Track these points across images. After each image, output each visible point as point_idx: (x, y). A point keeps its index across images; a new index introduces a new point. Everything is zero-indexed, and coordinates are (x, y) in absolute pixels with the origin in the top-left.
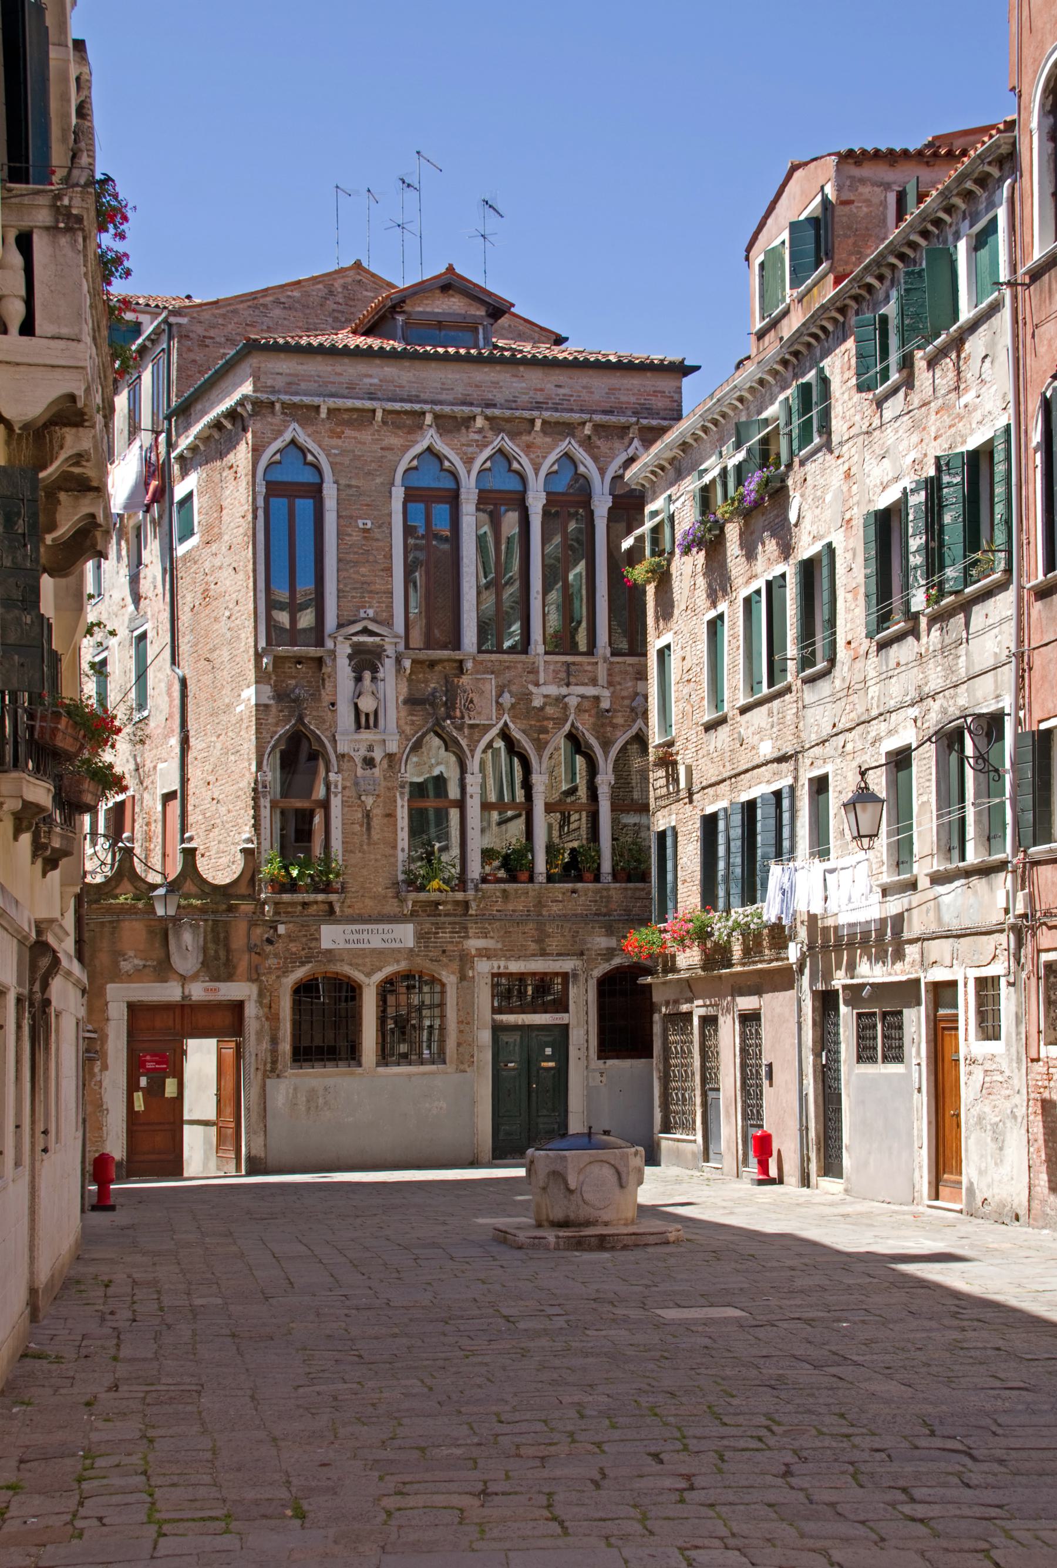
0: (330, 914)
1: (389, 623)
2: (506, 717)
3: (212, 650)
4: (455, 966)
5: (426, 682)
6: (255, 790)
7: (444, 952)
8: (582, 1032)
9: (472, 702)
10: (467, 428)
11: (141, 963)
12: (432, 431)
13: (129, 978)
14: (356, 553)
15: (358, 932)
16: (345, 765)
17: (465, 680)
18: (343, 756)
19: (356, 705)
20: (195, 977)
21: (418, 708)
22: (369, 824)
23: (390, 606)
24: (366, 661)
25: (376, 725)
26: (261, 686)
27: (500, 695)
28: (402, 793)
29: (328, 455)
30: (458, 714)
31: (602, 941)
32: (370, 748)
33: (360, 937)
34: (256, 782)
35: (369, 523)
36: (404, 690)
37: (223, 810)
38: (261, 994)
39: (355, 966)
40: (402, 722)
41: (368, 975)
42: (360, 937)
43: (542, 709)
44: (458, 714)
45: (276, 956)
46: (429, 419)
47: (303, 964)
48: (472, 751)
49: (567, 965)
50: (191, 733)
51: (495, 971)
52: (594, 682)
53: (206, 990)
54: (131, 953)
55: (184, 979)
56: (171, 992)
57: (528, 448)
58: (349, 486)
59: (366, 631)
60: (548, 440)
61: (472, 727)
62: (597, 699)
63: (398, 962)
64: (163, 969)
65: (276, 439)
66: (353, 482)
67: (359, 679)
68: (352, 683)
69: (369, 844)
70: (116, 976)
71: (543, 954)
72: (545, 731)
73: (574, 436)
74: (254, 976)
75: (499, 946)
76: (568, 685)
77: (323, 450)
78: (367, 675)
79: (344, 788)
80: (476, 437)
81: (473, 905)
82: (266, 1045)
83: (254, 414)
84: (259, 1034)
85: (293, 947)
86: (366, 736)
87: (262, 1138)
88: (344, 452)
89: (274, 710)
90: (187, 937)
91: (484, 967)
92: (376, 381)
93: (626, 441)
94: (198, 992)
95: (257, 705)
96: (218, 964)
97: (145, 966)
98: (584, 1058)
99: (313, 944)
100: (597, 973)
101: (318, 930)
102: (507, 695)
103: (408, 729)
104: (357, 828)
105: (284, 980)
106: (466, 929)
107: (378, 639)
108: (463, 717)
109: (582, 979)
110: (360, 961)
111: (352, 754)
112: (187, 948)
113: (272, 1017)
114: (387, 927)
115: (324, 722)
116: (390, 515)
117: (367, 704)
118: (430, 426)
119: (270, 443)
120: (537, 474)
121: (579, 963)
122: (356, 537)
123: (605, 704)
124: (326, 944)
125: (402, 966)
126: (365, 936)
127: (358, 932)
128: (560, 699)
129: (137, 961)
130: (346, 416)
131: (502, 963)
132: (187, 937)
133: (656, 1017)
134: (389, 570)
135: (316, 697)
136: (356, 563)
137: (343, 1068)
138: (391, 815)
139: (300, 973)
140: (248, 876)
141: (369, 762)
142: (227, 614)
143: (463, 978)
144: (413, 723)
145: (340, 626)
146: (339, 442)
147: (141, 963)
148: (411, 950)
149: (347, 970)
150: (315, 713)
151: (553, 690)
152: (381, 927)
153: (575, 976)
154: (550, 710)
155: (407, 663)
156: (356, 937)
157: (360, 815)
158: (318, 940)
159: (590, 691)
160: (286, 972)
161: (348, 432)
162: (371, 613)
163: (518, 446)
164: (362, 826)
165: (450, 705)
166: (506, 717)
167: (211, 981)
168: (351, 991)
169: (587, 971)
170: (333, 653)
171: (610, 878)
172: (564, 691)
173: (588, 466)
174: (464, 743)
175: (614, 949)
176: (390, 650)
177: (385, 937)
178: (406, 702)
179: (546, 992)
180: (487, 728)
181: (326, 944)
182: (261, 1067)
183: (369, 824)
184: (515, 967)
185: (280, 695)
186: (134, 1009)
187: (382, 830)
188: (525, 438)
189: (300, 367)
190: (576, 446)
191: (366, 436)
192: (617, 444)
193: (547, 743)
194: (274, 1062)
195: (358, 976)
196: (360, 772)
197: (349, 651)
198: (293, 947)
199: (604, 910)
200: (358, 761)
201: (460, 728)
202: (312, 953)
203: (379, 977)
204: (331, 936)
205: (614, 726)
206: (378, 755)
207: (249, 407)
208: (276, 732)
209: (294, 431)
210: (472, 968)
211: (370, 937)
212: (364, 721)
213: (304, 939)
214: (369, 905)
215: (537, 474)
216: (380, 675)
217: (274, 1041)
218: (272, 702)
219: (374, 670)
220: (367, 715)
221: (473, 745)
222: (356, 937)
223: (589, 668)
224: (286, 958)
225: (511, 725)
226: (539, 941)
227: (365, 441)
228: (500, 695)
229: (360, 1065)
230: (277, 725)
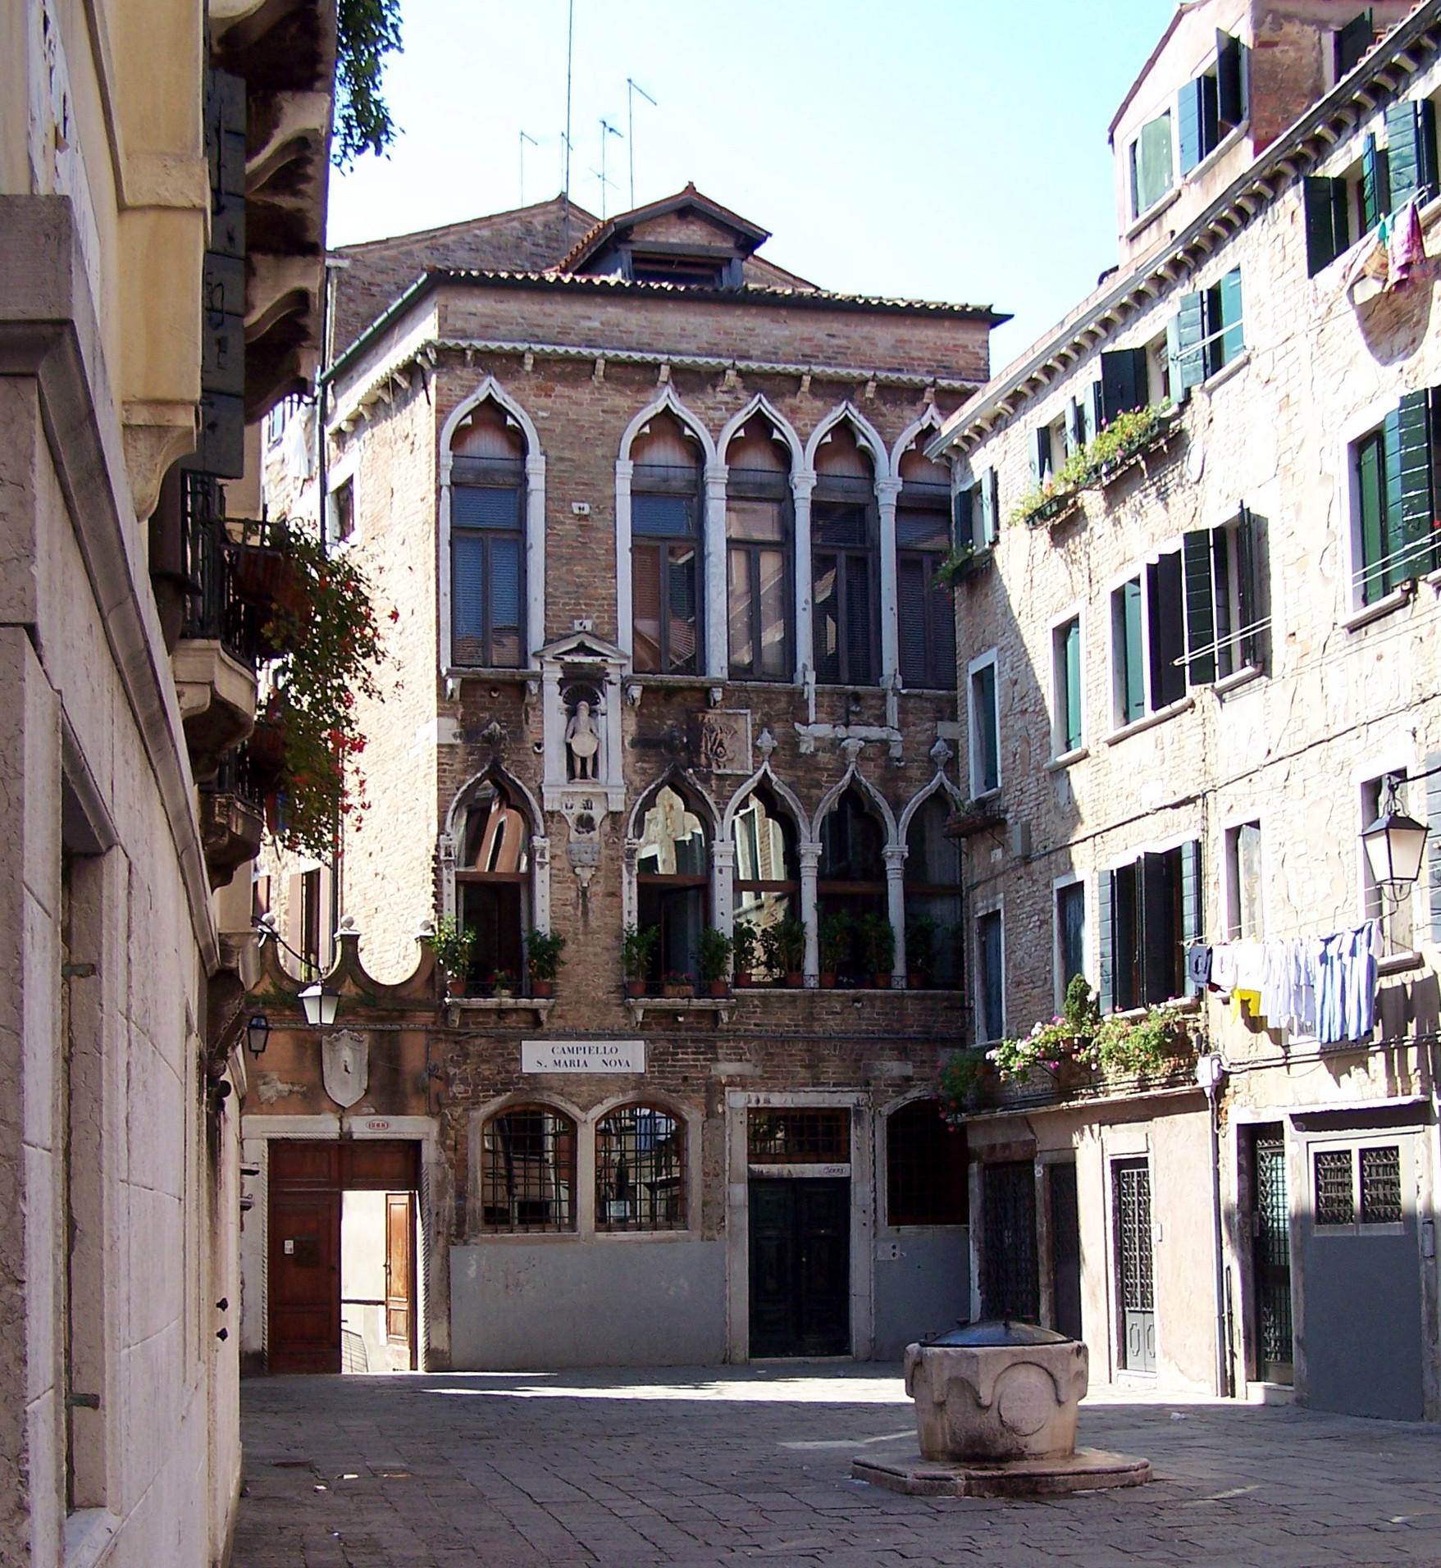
0: (535, 1026)
1: (611, 638)
4: (700, 1098)
5: (661, 717)
6: (435, 858)
7: (685, 1079)
8: (868, 1188)
9: (721, 745)
10: (714, 387)
11: (286, 1088)
12: (668, 390)
14: (569, 546)
15: (571, 1051)
16: (554, 827)
17: (711, 716)
18: (552, 813)
19: (569, 746)
20: (356, 1109)
21: (652, 752)
22: (585, 906)
23: (614, 619)
24: (582, 688)
25: (595, 774)
26: (444, 720)
29: (533, 419)
31: (893, 1068)
32: (588, 805)
33: (574, 1057)
34: (437, 848)
35: (586, 506)
36: (632, 725)
38: (443, 1132)
39: (569, 1096)
40: (629, 771)
42: (574, 1057)
43: (814, 755)
45: (464, 1081)
46: (665, 371)
47: (498, 1093)
48: (722, 811)
51: (753, 1105)
52: (882, 720)
54: (274, 1076)
55: (341, 1111)
56: (325, 1127)
57: (792, 413)
58: (561, 459)
59: (582, 649)
60: (819, 404)
62: (885, 744)
63: (623, 1091)
64: (313, 1097)
65: (466, 397)
66: (567, 454)
67: (572, 713)
68: (564, 718)
69: (585, 933)
72: (819, 786)
73: (851, 400)
75: (759, 1071)
76: (847, 725)
77: (528, 412)
78: (584, 706)
79: (553, 857)
80: (727, 398)
81: (725, 1016)
85: (486, 1070)
86: (580, 787)
87: (445, 1324)
88: (555, 415)
90: (347, 1054)
92: (596, 324)
93: (919, 406)
94: (362, 1127)
95: (439, 746)
96: (388, 1092)
97: (291, 1092)
98: (870, 1224)
99: (512, 1066)
100: (886, 1110)
102: (766, 735)
103: (637, 780)
105: (474, 1114)
106: (713, 1048)
108: (710, 765)
109: (867, 1117)
110: (573, 1089)
111: (564, 812)
113: (460, 1165)
114: (609, 1044)
115: (529, 768)
117: (584, 746)
118: (666, 383)
119: (458, 403)
120: (804, 448)
121: (861, 1095)
122: (570, 526)
123: (896, 752)
124: (529, 1066)
126: (581, 1056)
127: (571, 1051)
128: (835, 744)
129: (280, 1086)
130: (557, 370)
131: (762, 1096)
132: (347, 1054)
134: (613, 567)
135: (517, 735)
136: (570, 560)
138: (615, 894)
139: (494, 1104)
140: (426, 974)
141: (586, 823)
143: (710, 1114)
144: (644, 772)
146: (549, 402)
147: (286, 1088)
150: (514, 757)
151: (825, 730)
152: (601, 1044)
153: (859, 1113)
154: (823, 757)
155: (636, 692)
156: (568, 1057)
157: (574, 894)
158: (519, 1060)
159: (875, 733)
160: (476, 1104)
161: (559, 389)
163: (780, 411)
164: (576, 908)
166: (766, 765)
167: (377, 1113)
172: (841, 732)
173: (870, 436)
174: (710, 800)
175: (908, 1079)
176: (614, 675)
177: (607, 1058)
178: (633, 744)
180: (741, 780)
181: (529, 1066)
182: (444, 1230)
183: (585, 906)
185: (469, 732)
187: (603, 915)
188: (789, 401)
189: (500, 306)
190: (856, 412)
191: (584, 394)
192: (908, 412)
193: (820, 800)
194: (461, 1223)
195: (574, 1111)
196: (573, 835)
197: (560, 675)
199: (896, 1026)
201: (705, 780)
202: (511, 1078)
203: (598, 1111)
204: (537, 1056)
205: (909, 780)
206: (598, 813)
208: (463, 782)
209: (489, 386)
210: (722, 1102)
212: (579, 768)
213: (500, 1060)
214: (586, 1017)
215: (804, 448)
216: (601, 707)
218: (459, 741)
219: (594, 701)
220: (584, 760)
222: (568, 1057)
223: (873, 702)
224: (476, 1085)
225: (772, 776)
227: (585, 402)
230: (465, 771)
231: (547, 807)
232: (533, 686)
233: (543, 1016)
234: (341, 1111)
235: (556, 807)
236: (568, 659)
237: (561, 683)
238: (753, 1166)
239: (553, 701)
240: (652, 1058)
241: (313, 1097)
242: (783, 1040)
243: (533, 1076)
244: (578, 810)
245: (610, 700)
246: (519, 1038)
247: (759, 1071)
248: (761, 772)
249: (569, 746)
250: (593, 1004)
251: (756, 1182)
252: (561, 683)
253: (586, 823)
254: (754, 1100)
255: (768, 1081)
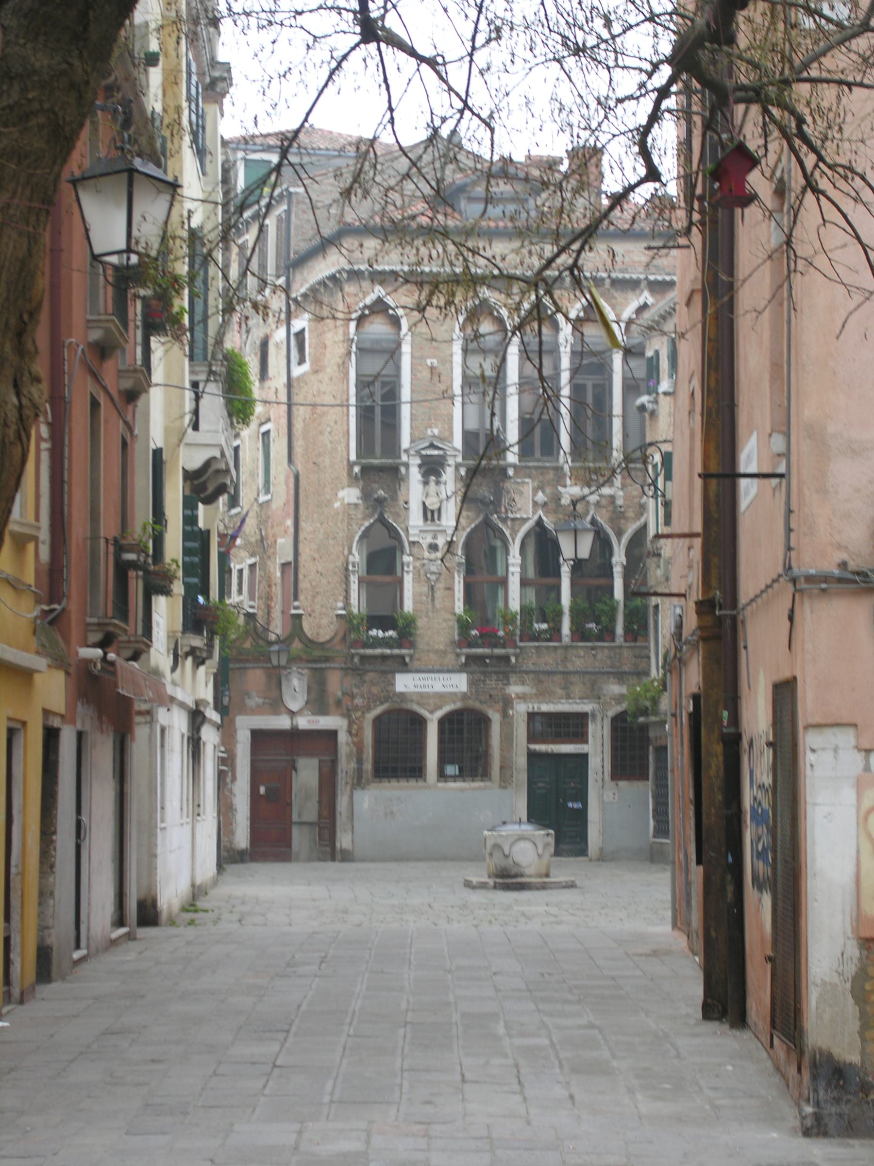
2: (540, 512)
3: (319, 455)
8: (599, 760)
13: (254, 712)
17: (508, 485)
18: (414, 543)
19: (424, 503)
20: (300, 712)
24: (432, 468)
27: (534, 495)
28: (459, 571)
30: (503, 509)
32: (435, 537)
33: (426, 683)
37: (324, 581)
41: (432, 712)
42: (426, 683)
44: (503, 509)
45: (362, 696)
47: (382, 703)
48: (513, 540)
49: (586, 707)
50: (843, 77)
53: (309, 722)
55: (292, 714)
56: (283, 723)
59: (432, 446)
61: (514, 520)
63: (454, 702)
64: (276, 705)
67: (426, 483)
70: (244, 710)
71: (568, 697)
74: (347, 715)
81: (513, 659)
82: (353, 765)
83: (349, 279)
84: (349, 756)
85: (375, 690)
89: (361, 508)
90: (295, 682)
91: (521, 709)
94: (304, 723)
96: (319, 702)
99: (390, 688)
100: (611, 713)
101: (394, 678)
104: (424, 598)
106: (508, 679)
107: (441, 452)
108: (507, 512)
109: (599, 718)
111: (421, 541)
112: (296, 689)
114: (446, 676)
116: (451, 355)
121: (596, 706)
125: (458, 705)
126: (430, 682)
129: (257, 699)
132: (295, 682)
133: (651, 748)
137: (412, 783)
138: (450, 588)
141: (433, 547)
142: (329, 429)
145: (412, 441)
148: (465, 694)
149: (416, 708)
152: (441, 676)
153: (594, 715)
156: (422, 683)
158: (393, 685)
160: (369, 709)
162: (436, 432)
165: (496, 504)
168: (418, 723)
169: (603, 711)
170: (407, 465)
171: (622, 640)
174: (507, 533)
176: (451, 461)
179: (572, 726)
183: (433, 596)
184: (545, 708)
186: (257, 736)
195: (425, 713)
198: (375, 690)
200: (425, 546)
201: (504, 520)
202: (389, 694)
203: (439, 714)
204: (404, 683)
207: (345, 275)
210: (512, 708)
211: (433, 683)
212: (430, 514)
216: (444, 477)
217: (360, 761)
219: (438, 475)
220: (432, 512)
221: (514, 533)
222: (422, 683)
226: (564, 688)
228: (534, 495)
229: (425, 781)
230: (364, 519)
231: (412, 539)
232: (403, 470)
233: (407, 660)
234: (292, 714)
235: (416, 539)
236: (423, 452)
237: (420, 466)
238: (533, 747)
239: (415, 475)
240: (471, 683)
241: (276, 705)
242: (549, 673)
243: (402, 694)
244: (429, 540)
245: (449, 475)
246: (393, 672)
247: (534, 691)
248: (536, 517)
249: (424, 503)
250: (437, 652)
251: (532, 756)
252: (420, 466)
253: (433, 547)
254: (531, 706)
255: (543, 694)
